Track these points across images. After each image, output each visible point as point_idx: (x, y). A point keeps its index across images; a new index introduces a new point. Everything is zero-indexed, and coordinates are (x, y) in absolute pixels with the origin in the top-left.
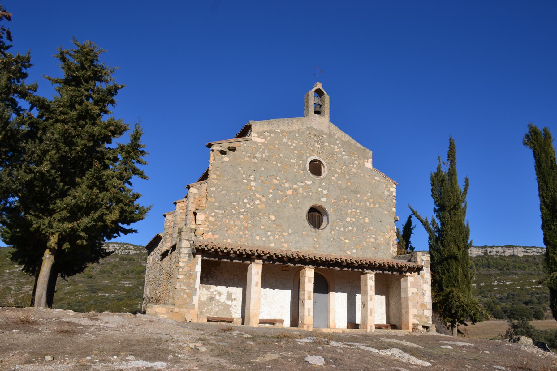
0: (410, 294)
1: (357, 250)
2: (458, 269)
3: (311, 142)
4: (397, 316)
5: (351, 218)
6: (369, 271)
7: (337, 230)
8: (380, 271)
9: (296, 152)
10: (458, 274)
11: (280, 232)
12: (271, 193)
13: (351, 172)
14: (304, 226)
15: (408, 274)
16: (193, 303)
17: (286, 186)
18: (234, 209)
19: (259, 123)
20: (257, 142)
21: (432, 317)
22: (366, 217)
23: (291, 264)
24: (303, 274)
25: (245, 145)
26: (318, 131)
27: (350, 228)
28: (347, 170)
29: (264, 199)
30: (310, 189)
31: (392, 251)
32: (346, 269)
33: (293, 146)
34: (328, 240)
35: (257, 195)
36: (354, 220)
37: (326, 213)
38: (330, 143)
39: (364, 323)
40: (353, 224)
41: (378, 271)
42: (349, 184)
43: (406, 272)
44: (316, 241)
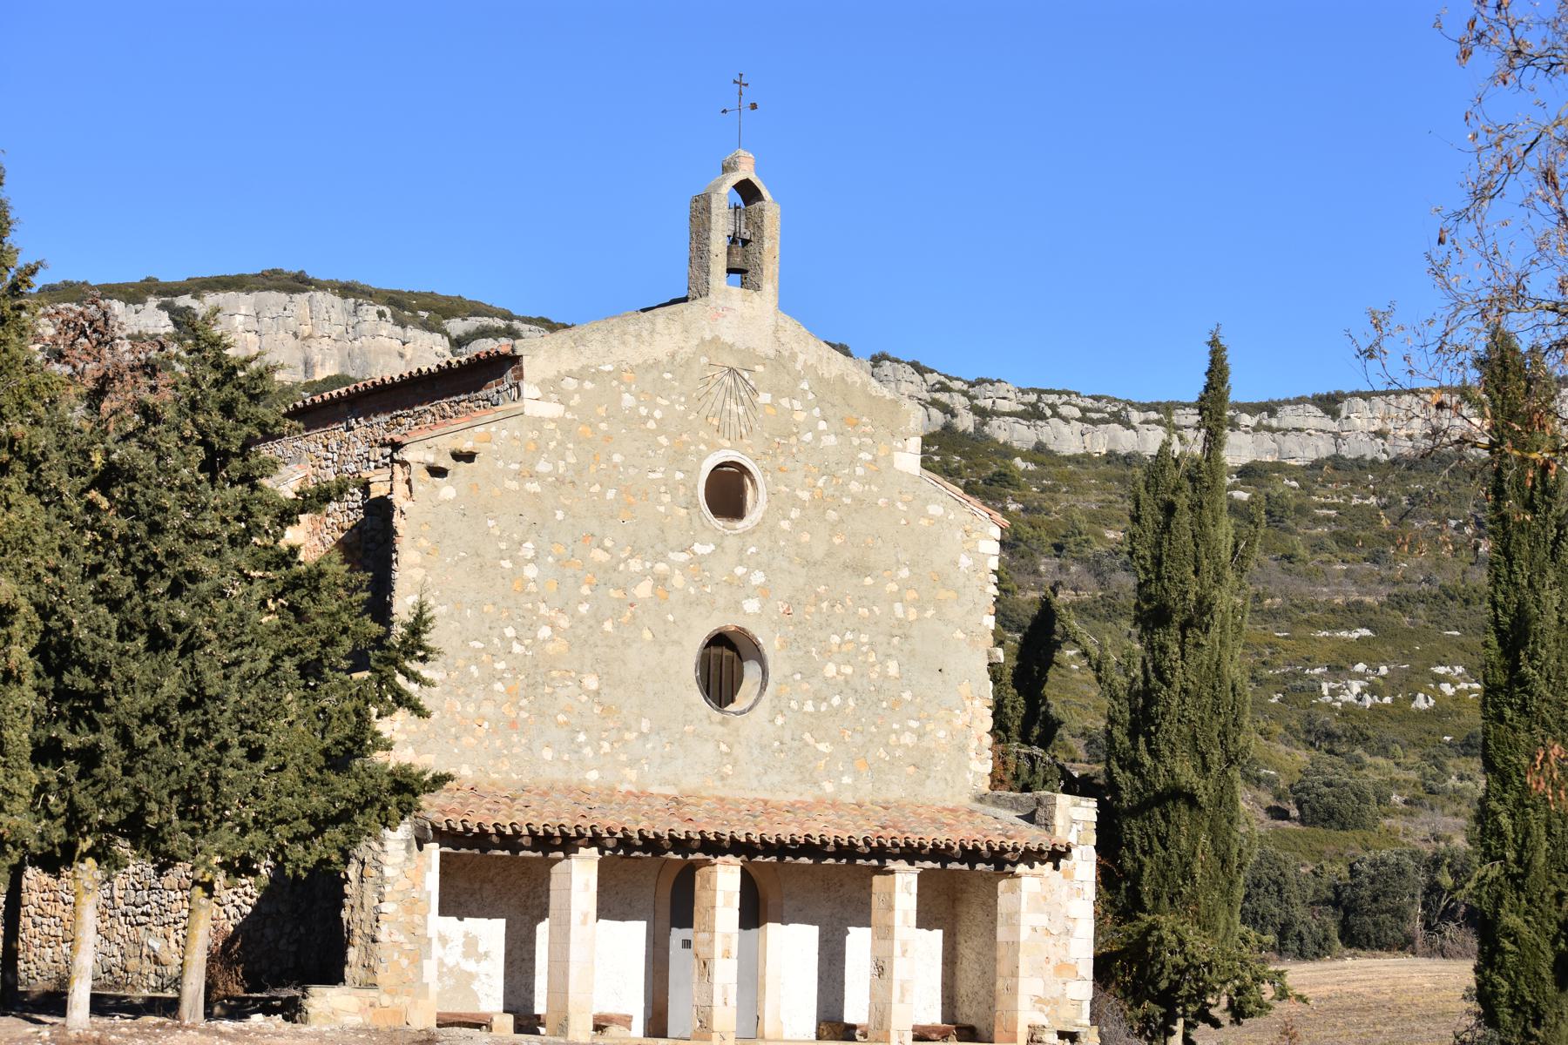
0: (1025, 934)
1: (857, 775)
2: (1196, 838)
3: (712, 398)
4: (980, 999)
5: (838, 665)
6: (901, 865)
7: (793, 710)
8: (935, 862)
9: (663, 440)
10: (1194, 854)
11: (615, 731)
12: (586, 599)
13: (847, 496)
14: (687, 706)
15: (1021, 868)
16: (425, 981)
17: (632, 569)
18: (477, 664)
19: (545, 347)
20: (541, 419)
21: (1093, 1002)
22: (889, 656)
23: (676, 853)
24: (709, 881)
25: (504, 433)
26: (740, 351)
27: (836, 701)
28: (831, 491)
29: (564, 622)
30: (707, 573)
31: (976, 773)
32: (831, 861)
33: (656, 420)
34: (763, 747)
35: (543, 609)
36: (848, 670)
37: (758, 655)
38: (777, 393)
39: (881, 1024)
40: (846, 687)
41: (928, 864)
42: (837, 541)
43: (1014, 864)
44: (727, 754)
